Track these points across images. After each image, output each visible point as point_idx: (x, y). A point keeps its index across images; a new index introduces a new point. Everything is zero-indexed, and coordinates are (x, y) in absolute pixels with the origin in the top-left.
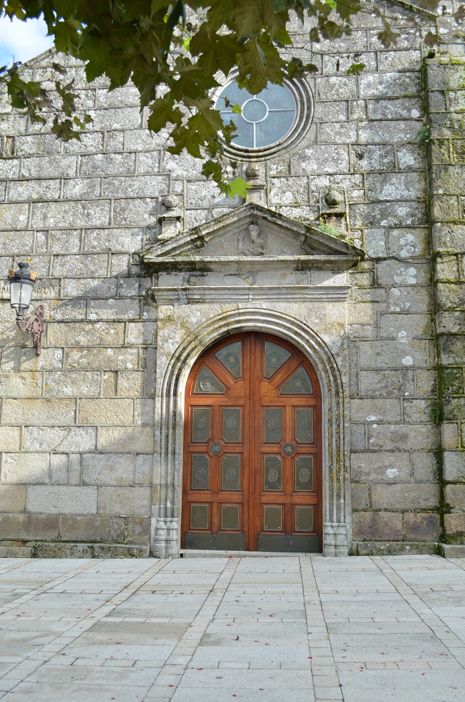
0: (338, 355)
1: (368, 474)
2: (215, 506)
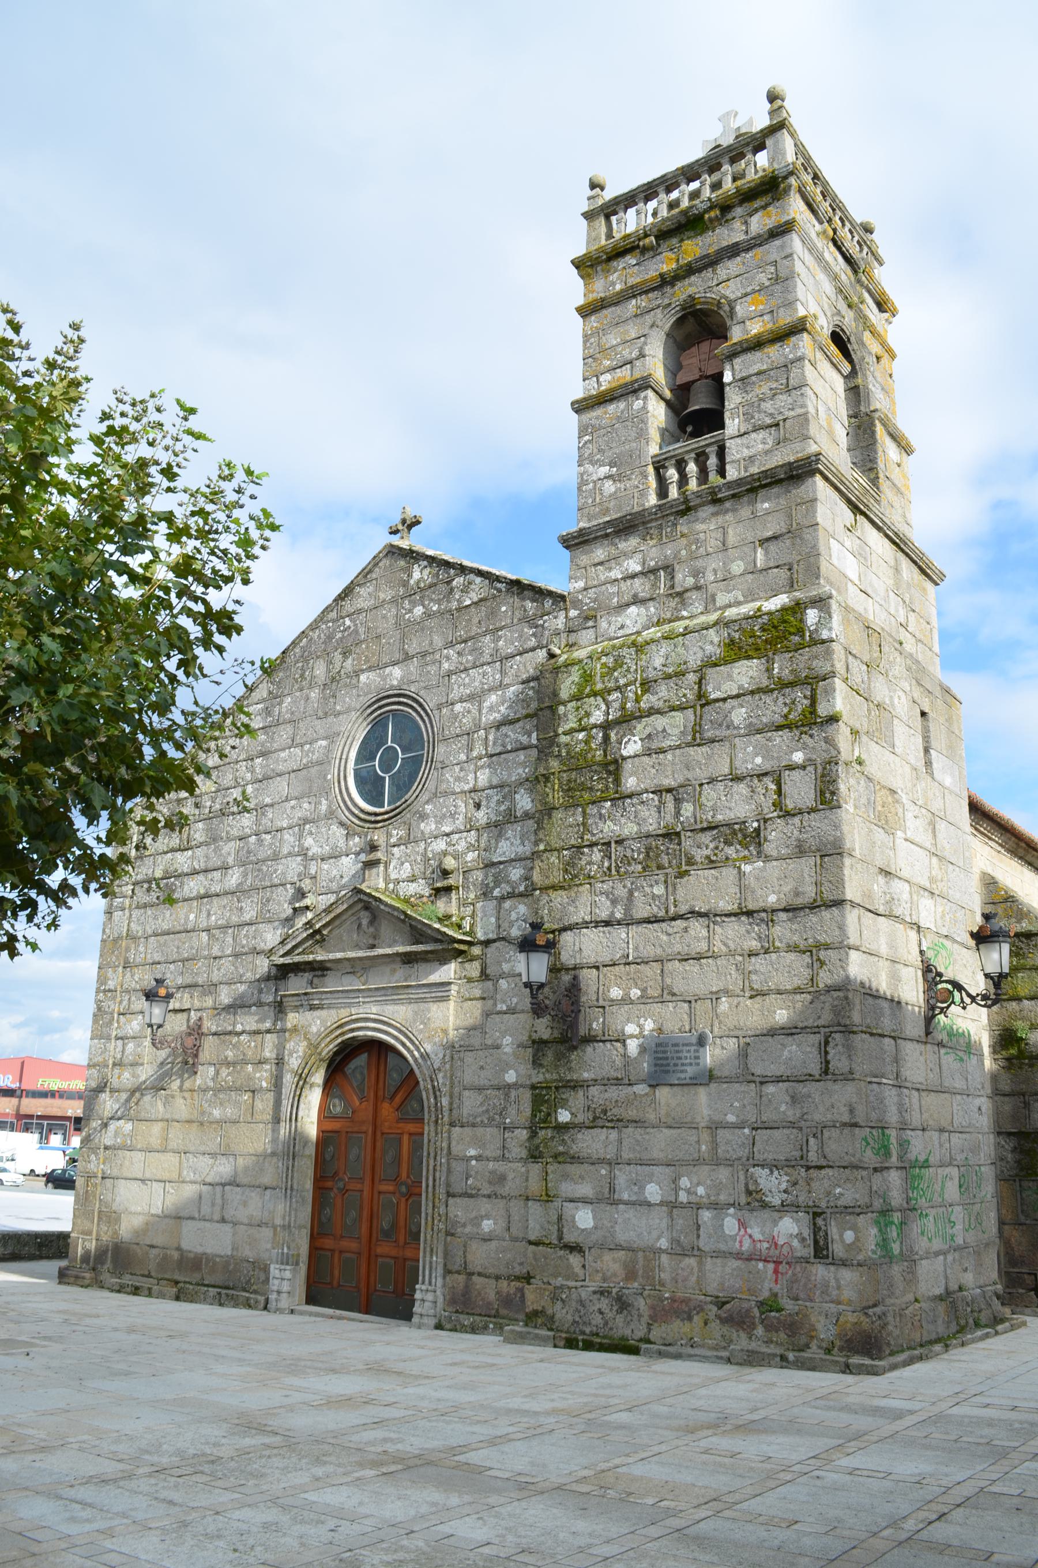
0: (439, 1070)
1: (464, 1225)
2: (337, 1255)
